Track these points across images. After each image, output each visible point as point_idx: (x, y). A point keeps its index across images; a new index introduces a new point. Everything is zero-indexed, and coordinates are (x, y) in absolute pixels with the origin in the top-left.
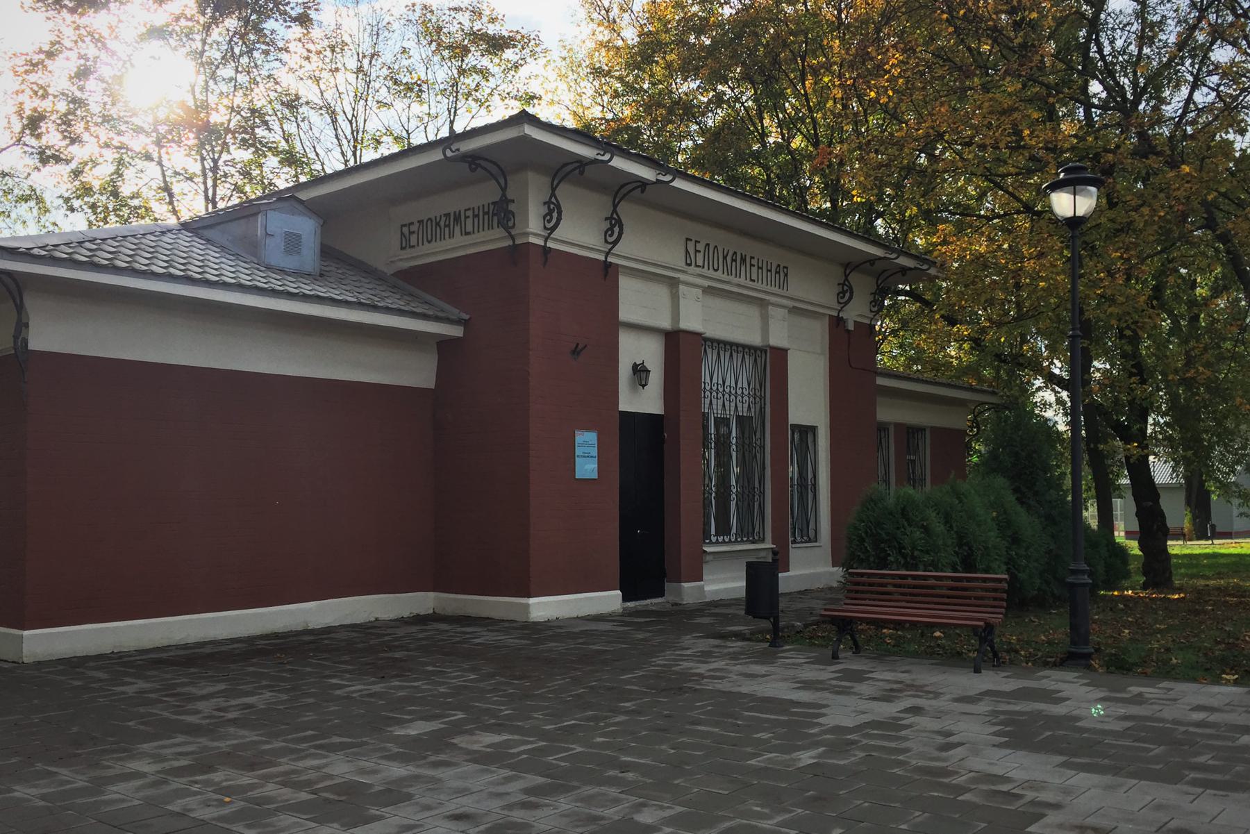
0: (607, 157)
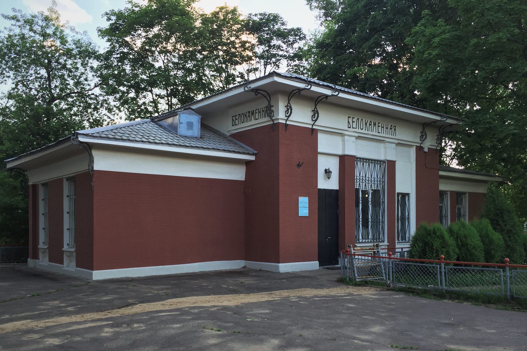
0: (309, 87)
